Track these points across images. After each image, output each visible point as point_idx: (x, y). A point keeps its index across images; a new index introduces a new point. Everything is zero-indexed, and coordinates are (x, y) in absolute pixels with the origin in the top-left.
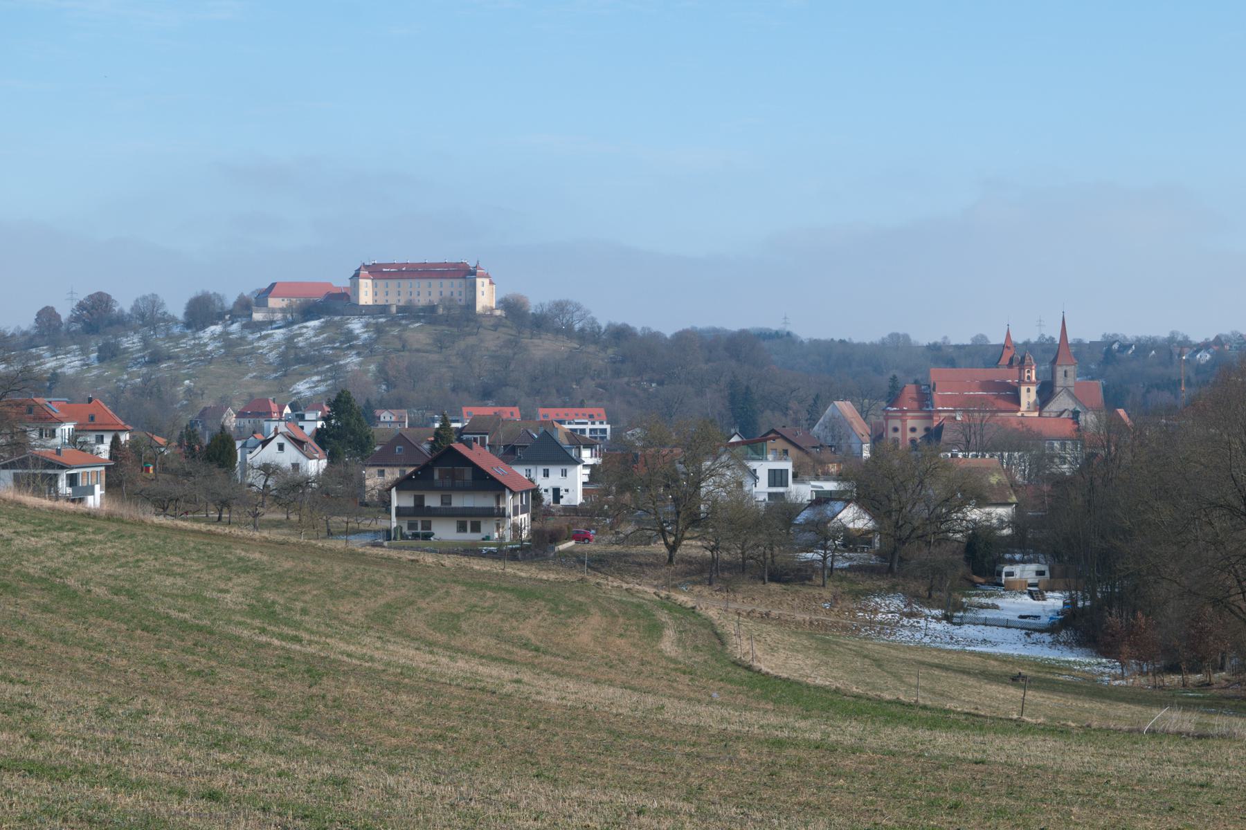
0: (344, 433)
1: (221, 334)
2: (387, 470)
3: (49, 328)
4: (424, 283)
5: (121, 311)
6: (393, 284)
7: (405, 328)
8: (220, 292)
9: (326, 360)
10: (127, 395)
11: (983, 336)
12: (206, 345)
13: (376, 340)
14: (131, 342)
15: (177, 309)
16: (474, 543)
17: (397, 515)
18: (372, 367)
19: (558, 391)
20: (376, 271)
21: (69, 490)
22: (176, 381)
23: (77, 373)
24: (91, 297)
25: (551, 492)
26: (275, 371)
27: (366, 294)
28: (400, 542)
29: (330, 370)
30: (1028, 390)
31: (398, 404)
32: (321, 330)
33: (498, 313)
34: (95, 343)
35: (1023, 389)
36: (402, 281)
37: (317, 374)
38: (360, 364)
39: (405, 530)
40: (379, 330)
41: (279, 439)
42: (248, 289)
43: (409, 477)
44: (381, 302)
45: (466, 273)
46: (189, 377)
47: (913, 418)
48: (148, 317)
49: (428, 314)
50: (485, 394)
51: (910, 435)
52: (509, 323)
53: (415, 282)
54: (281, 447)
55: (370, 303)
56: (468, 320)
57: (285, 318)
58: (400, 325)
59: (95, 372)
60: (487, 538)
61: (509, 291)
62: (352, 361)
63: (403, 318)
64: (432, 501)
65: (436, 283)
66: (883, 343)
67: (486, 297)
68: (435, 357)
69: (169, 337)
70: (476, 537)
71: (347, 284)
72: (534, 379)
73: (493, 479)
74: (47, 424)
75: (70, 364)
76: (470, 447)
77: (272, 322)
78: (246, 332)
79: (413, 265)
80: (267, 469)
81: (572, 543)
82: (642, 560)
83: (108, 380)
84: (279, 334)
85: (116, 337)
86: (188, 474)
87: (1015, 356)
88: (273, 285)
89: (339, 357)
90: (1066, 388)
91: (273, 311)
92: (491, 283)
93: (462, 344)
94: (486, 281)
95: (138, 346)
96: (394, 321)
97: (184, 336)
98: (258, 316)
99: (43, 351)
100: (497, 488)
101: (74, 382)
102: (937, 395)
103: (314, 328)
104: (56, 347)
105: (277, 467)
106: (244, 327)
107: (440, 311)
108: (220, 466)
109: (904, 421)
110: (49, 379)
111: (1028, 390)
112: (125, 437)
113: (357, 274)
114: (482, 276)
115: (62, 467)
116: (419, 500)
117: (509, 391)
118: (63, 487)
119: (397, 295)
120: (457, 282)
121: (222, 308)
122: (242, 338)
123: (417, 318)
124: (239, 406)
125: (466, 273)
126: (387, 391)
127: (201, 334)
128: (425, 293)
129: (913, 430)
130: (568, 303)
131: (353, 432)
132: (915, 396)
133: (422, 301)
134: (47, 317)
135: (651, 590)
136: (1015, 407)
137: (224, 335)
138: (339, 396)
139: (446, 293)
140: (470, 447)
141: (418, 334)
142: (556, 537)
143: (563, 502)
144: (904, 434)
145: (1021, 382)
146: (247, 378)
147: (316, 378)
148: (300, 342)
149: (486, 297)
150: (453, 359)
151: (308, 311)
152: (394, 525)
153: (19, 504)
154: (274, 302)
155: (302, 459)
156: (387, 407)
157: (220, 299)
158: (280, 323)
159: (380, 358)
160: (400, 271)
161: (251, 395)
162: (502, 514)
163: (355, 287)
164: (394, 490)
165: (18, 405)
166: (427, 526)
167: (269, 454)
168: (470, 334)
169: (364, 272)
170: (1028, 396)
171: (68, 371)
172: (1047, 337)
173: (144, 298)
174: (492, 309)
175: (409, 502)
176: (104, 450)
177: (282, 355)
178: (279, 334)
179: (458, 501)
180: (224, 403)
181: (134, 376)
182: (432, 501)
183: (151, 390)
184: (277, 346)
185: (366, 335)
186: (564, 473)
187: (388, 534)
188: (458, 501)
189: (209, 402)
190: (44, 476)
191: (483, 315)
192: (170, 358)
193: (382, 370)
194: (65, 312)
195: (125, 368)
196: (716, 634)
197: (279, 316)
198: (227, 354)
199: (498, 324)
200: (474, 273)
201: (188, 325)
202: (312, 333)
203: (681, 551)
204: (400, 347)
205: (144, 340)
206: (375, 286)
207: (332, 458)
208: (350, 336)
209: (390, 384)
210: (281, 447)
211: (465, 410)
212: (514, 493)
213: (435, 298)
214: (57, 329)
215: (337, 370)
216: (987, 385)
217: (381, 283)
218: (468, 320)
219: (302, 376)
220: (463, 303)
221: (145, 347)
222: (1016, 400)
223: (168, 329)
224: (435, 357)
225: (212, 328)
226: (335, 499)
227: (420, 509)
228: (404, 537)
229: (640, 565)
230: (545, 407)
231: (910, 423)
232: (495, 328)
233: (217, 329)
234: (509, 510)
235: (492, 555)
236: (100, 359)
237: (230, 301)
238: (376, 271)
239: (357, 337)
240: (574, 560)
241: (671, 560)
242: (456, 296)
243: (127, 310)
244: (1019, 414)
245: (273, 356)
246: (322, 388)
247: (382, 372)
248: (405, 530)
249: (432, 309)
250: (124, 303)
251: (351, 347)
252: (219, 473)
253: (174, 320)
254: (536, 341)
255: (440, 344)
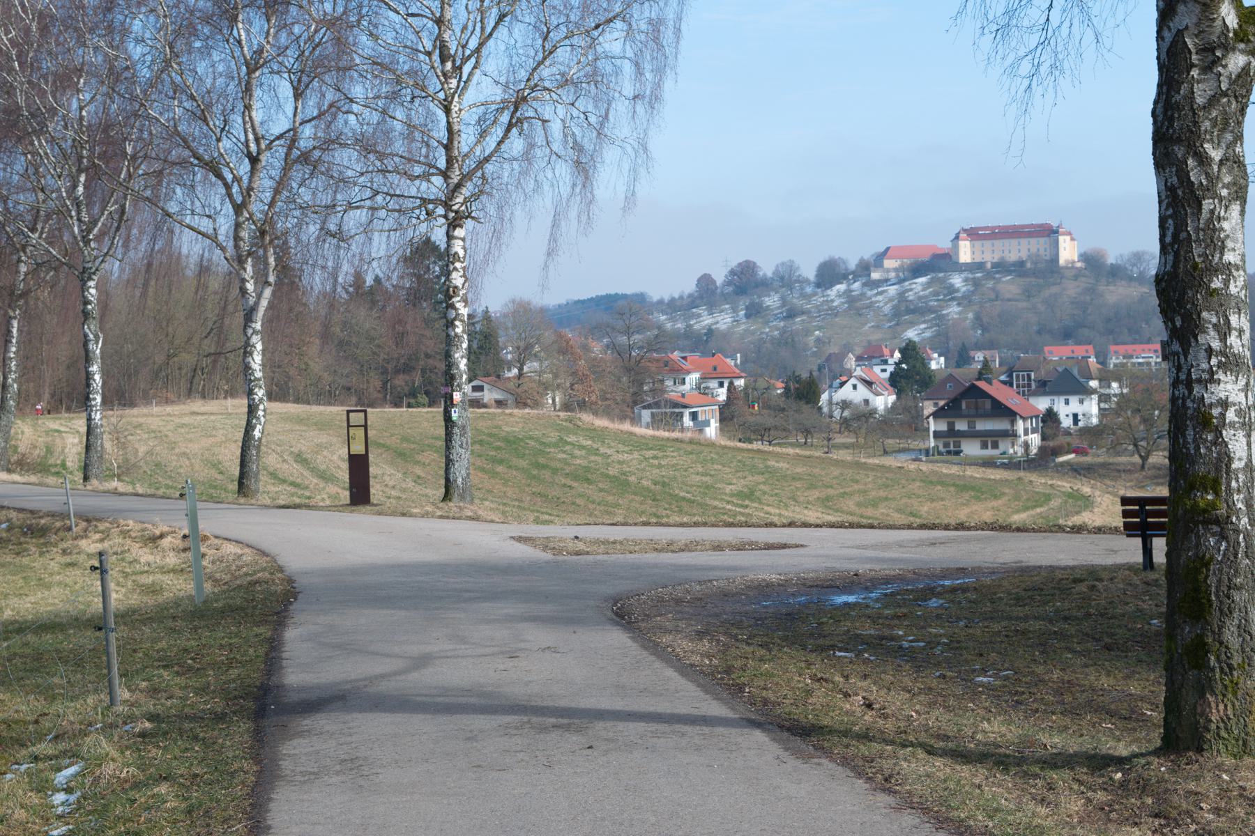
0: (910, 377)
1: (845, 292)
3: (707, 293)
4: (1014, 242)
5: (765, 275)
6: (988, 243)
7: (998, 281)
8: (844, 257)
9: (931, 310)
10: (768, 345)
12: (832, 301)
13: (973, 292)
14: (772, 301)
15: (810, 272)
16: (992, 457)
17: (935, 437)
18: (970, 315)
19: (1129, 330)
20: (973, 234)
21: (691, 424)
22: (808, 332)
23: (729, 328)
24: (740, 264)
25: (1071, 417)
26: (890, 321)
27: (966, 253)
28: (937, 457)
29: (934, 319)
31: (991, 345)
32: (928, 285)
33: (1079, 265)
34: (743, 303)
37: (924, 322)
38: (960, 313)
39: (941, 448)
40: (976, 283)
41: (853, 381)
42: (868, 254)
43: (942, 408)
44: (978, 260)
45: (1050, 232)
46: (819, 328)
48: (786, 279)
49: (1018, 268)
50: (1067, 335)
52: (1087, 273)
53: (1006, 242)
54: (855, 387)
55: (969, 261)
56: (1053, 272)
57: (897, 276)
59: (743, 327)
60: (1004, 453)
61: (1090, 245)
62: (953, 310)
63: (998, 272)
64: (961, 426)
65: (1024, 241)
67: (1068, 252)
68: (1024, 304)
69: (804, 296)
70: (995, 452)
71: (949, 245)
72: (1109, 320)
73: (1006, 407)
74: (679, 374)
75: (723, 320)
76: (990, 383)
77: (887, 280)
78: (866, 289)
80: (845, 404)
81: (1073, 456)
82: (1122, 467)
83: (753, 333)
85: (760, 297)
86: (784, 409)
88: (888, 249)
89: (942, 308)
91: (888, 271)
92: (1072, 239)
93: (1046, 293)
94: (1068, 238)
95: (778, 304)
96: (989, 275)
97: (815, 294)
98: (875, 276)
99: (702, 310)
100: (1011, 415)
101: (725, 335)
103: (922, 284)
104: (712, 308)
105: (851, 403)
106: (864, 285)
107: (1029, 265)
108: (807, 403)
110: (706, 334)
112: (740, 383)
113: (957, 237)
114: (1064, 234)
115: (685, 407)
116: (951, 426)
117: (1085, 332)
118: (687, 421)
119: (991, 253)
120: (1042, 240)
121: (846, 269)
122: (863, 294)
123: (1009, 272)
124: (859, 351)
125: (1050, 232)
126: (982, 335)
127: (829, 292)
128: (1015, 251)
130: (1144, 253)
131: (918, 373)
133: (1013, 257)
134: (705, 282)
135: (1068, 485)
137: (848, 292)
138: (907, 345)
139: (1034, 250)
140: (990, 383)
141: (1009, 286)
142: (1056, 452)
143: (1081, 424)
146: (867, 327)
147: (923, 326)
148: (911, 296)
149: (1068, 252)
150: (1039, 305)
151: (917, 270)
152: (932, 444)
153: (631, 433)
154: (889, 263)
155: (870, 396)
156: (979, 347)
157: (844, 262)
158: (894, 281)
159: (976, 308)
160: (993, 233)
161: (869, 342)
162: (1014, 435)
163: (956, 247)
164: (931, 419)
165: (658, 360)
166: (957, 445)
167: (846, 393)
168: (1054, 284)
171: (722, 326)
173: (783, 264)
174: (1073, 262)
175: (943, 427)
176: (722, 394)
177: (895, 308)
178: (892, 290)
179: (981, 425)
180: (847, 349)
181: (772, 329)
182: (961, 426)
183: (787, 341)
184: (891, 300)
185: (964, 289)
186: (1081, 402)
187: (927, 452)
188: (981, 425)
189: (834, 349)
190: (673, 413)
191: (1067, 268)
192: (803, 313)
193: (978, 318)
194: (720, 277)
195: (767, 323)
197: (892, 275)
198: (849, 308)
199: (1078, 274)
200: (1057, 232)
201: (818, 285)
202: (920, 288)
203: (1151, 460)
204: (993, 297)
205: (783, 299)
206: (973, 246)
207: (899, 394)
208: (952, 290)
209: (985, 329)
210: (855, 387)
211: (848, 366)
212: (1024, 419)
213: (1024, 255)
214: (713, 292)
215: (941, 318)
217: (978, 243)
218: (1053, 272)
219: (912, 324)
220: (1048, 258)
221: (783, 305)
223: (802, 289)
224: (1024, 304)
225: (838, 287)
226: (903, 423)
227: (952, 432)
228: (940, 453)
229: (1119, 471)
230: (1117, 344)
232: (1076, 277)
233: (841, 287)
234: (1021, 431)
235: (1004, 466)
236: (748, 316)
237: (852, 265)
238: (973, 234)
239: (957, 291)
240: (1077, 471)
241: (1143, 467)
242: (1042, 252)
243: (769, 274)
245: (887, 309)
246: (928, 334)
247: (979, 321)
248: (941, 448)
249: (1021, 264)
250: (767, 269)
251: (953, 299)
252: (806, 408)
253: (807, 281)
254: (1111, 288)
255: (1028, 294)
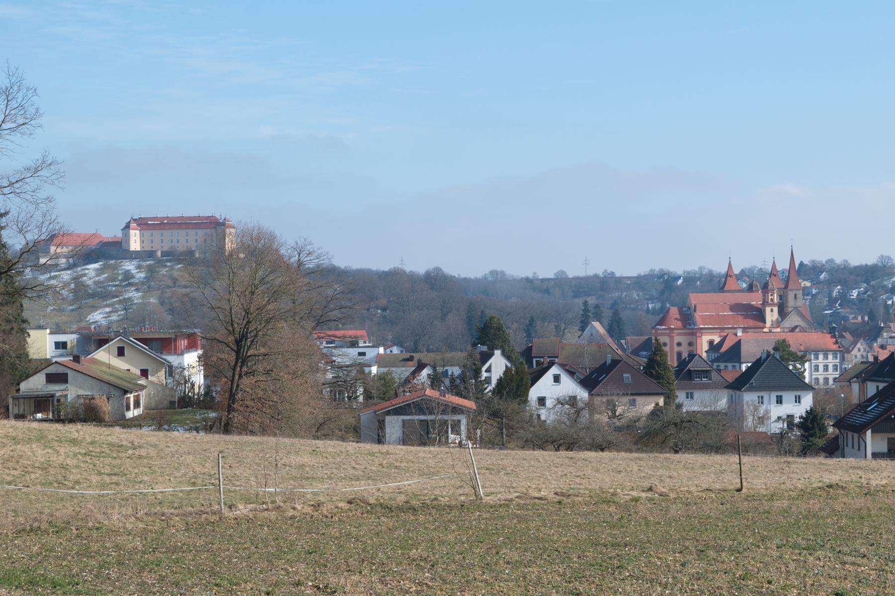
2: (640, 400)
4: (182, 232)
6: (157, 233)
11: (563, 272)
20: (142, 223)
27: (135, 243)
30: (772, 311)
32: (99, 272)
35: (768, 309)
36: (153, 231)
37: (107, 306)
41: (554, 370)
44: (147, 248)
47: (679, 334)
51: (676, 349)
54: (557, 379)
55: (138, 249)
58: (166, 266)
62: (133, 295)
63: (170, 261)
65: (192, 232)
66: (485, 278)
71: (119, 235)
79: (172, 218)
84: (66, 276)
87: (759, 281)
90: (796, 308)
102: (698, 315)
103: (96, 270)
109: (672, 338)
111: (772, 311)
113: (127, 227)
119: (163, 242)
123: (179, 261)
129: (679, 344)
132: (678, 317)
133: (181, 247)
136: (761, 324)
144: (672, 348)
145: (765, 303)
147: (108, 310)
151: (89, 256)
160: (162, 224)
163: (126, 236)
169: (133, 225)
170: (771, 315)
172: (609, 271)
196: (400, 509)
197: (63, 261)
206: (142, 236)
208: (128, 275)
210: (557, 379)
216: (733, 308)
217: (148, 233)
219: (95, 308)
222: (763, 320)
231: (677, 339)
244: (766, 330)
251: (130, 285)
